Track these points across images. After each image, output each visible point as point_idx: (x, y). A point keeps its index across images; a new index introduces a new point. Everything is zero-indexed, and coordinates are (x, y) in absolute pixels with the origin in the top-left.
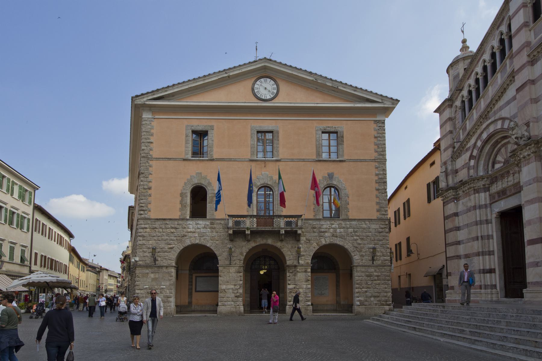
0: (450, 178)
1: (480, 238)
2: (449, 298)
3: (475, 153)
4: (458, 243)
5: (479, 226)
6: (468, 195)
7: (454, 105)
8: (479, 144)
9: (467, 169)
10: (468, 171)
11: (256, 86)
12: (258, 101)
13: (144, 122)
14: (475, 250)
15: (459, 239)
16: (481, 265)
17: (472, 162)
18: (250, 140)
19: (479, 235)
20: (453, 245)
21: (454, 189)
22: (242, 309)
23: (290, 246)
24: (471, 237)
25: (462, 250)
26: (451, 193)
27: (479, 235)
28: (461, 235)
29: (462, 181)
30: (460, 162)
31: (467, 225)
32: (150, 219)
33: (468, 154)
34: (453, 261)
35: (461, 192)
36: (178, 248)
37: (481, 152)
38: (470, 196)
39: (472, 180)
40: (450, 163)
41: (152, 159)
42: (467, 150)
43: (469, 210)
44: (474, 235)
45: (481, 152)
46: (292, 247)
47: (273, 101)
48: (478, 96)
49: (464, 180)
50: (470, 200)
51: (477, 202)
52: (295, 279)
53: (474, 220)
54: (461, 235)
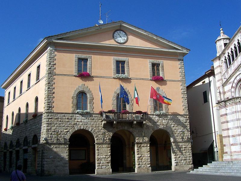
0: (222, 95)
1: (239, 127)
2: (225, 158)
3: (234, 85)
4: (228, 129)
5: (238, 121)
6: (231, 105)
7: (221, 60)
8: (236, 81)
9: (230, 92)
10: (231, 94)
11: (115, 35)
12: (118, 44)
13: (28, 160)
14: (237, 133)
15: (229, 127)
16: (237, 109)
17: (233, 90)
18: (113, 66)
19: (237, 113)
20: (226, 130)
21: (225, 101)
22: (111, 170)
23: (137, 131)
24: (235, 126)
25: (231, 133)
26: (223, 103)
27: (237, 113)
28: (230, 125)
29: (228, 98)
30: (228, 87)
31: (232, 120)
32: (53, 113)
33: (231, 85)
34: (226, 138)
35: (228, 104)
36: (71, 131)
37: (237, 85)
38: (233, 106)
39: (233, 98)
40: (222, 88)
41: (55, 75)
42: (230, 83)
43: (233, 113)
44: (236, 126)
45: (237, 85)
46: (139, 131)
47: (125, 45)
48: (233, 59)
49: (229, 98)
50: (233, 108)
51: (237, 109)
52: (141, 151)
53: (236, 118)
54: (230, 125)
